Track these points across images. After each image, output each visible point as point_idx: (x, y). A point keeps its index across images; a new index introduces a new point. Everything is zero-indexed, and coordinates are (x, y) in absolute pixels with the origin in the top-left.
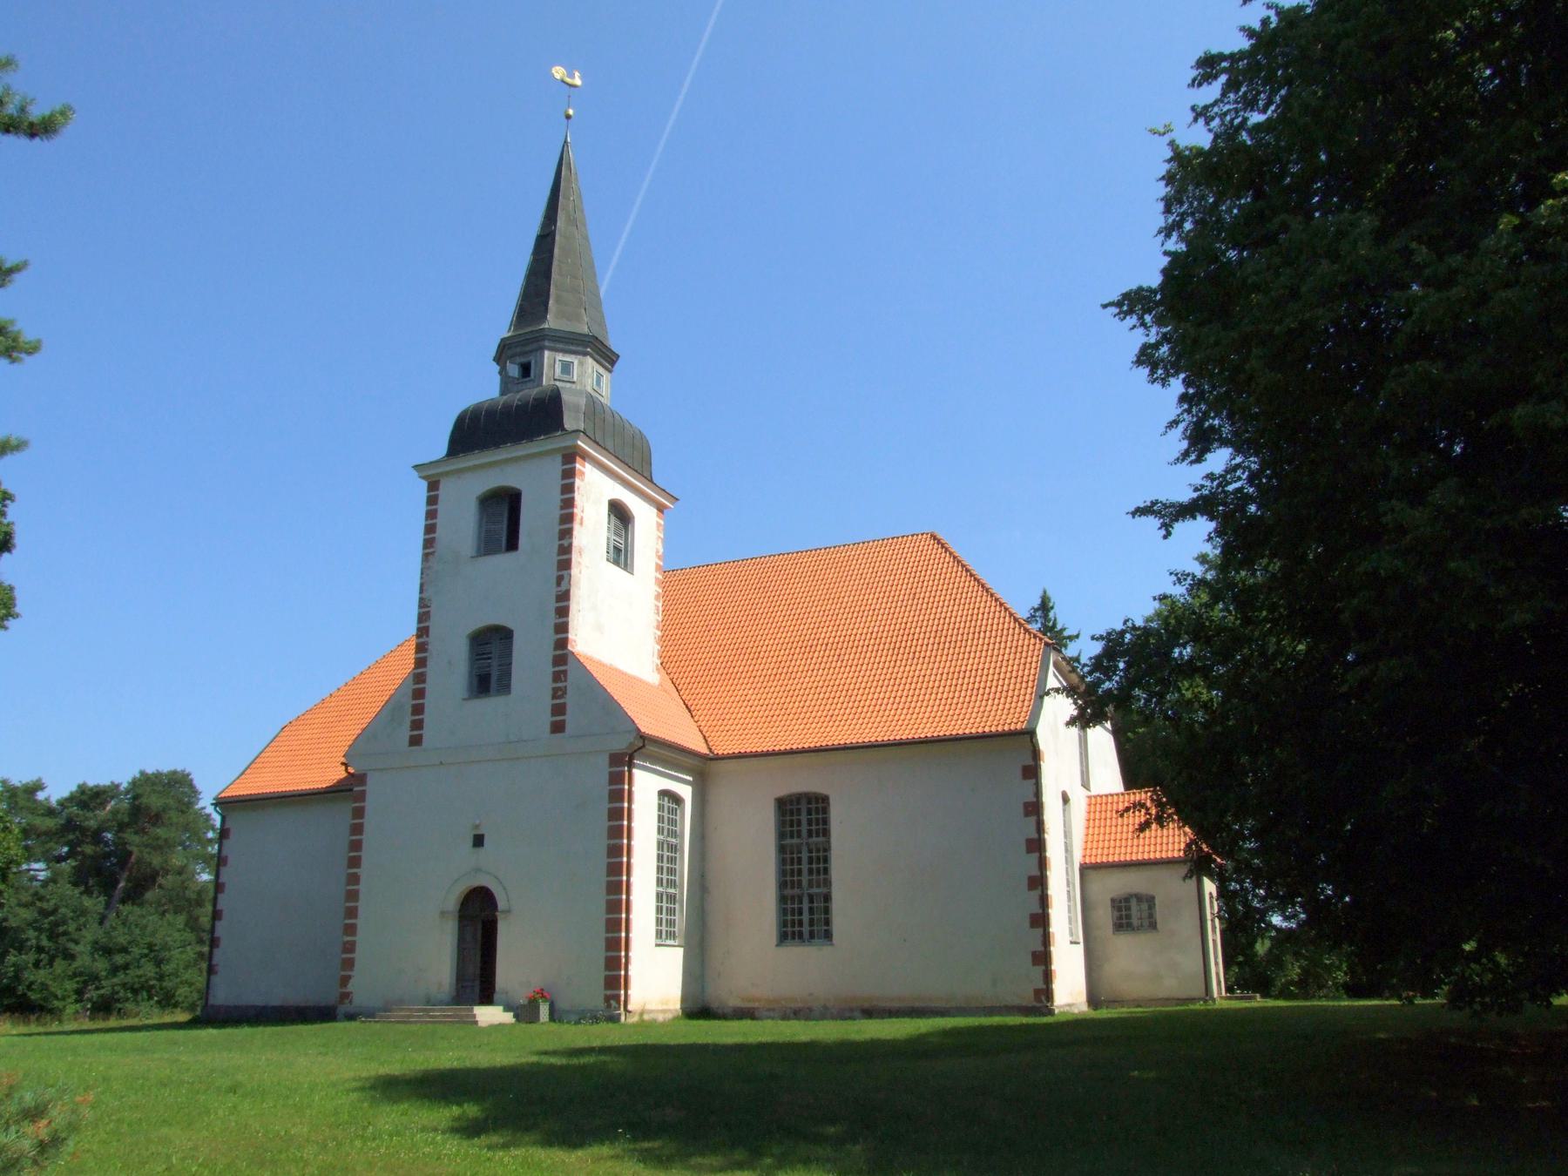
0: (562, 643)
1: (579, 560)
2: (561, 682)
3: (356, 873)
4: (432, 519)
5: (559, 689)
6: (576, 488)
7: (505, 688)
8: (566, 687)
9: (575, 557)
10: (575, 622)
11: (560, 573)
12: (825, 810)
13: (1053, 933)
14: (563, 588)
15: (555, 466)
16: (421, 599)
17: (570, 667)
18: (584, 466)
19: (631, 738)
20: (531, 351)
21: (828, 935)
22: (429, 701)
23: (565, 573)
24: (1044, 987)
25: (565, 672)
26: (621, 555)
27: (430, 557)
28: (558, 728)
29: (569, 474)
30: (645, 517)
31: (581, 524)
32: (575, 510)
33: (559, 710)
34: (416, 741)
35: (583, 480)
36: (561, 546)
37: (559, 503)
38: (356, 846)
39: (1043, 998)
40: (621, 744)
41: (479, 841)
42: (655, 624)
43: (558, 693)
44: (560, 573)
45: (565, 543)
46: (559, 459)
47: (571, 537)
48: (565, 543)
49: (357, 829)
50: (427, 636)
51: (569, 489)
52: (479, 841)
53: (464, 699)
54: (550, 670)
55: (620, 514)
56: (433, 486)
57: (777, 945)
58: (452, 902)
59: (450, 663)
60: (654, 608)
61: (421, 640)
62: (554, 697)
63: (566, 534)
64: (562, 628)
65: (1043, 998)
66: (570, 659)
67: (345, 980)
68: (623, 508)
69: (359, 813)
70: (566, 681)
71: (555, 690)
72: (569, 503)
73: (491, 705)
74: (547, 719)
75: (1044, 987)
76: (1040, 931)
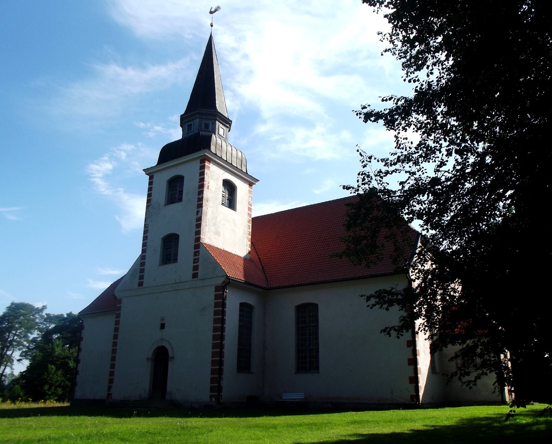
0: (198, 239)
1: (207, 204)
2: (197, 256)
3: (116, 342)
4: (150, 191)
5: (196, 259)
6: (205, 173)
7: (175, 260)
8: (199, 258)
9: (204, 202)
10: (204, 230)
11: (198, 209)
12: (179, 202)
13: (420, 368)
14: (199, 216)
15: (197, 164)
16: (145, 224)
17: (201, 250)
18: (210, 165)
19: (223, 279)
20: (192, 120)
21: (317, 368)
22: (146, 267)
23: (200, 209)
24: (415, 394)
25: (198, 252)
26: (231, 203)
27: (149, 207)
28: (195, 276)
29: (203, 167)
30: (241, 187)
31: (208, 188)
32: (205, 183)
33: (196, 268)
34: (141, 284)
35: (209, 170)
36: (199, 198)
37: (198, 180)
38: (116, 330)
39: (415, 400)
40: (220, 281)
41: (163, 326)
42: (248, 233)
43: (196, 261)
44: (198, 209)
45: (200, 196)
46: (199, 161)
47: (203, 194)
48: (200, 196)
49: (117, 323)
50: (147, 240)
51: (202, 174)
52: (163, 326)
53: (159, 265)
54: (193, 251)
55: (229, 186)
56: (151, 178)
57: (295, 373)
58: (150, 355)
59: (155, 250)
60: (247, 226)
61: (144, 242)
62: (194, 263)
63: (201, 192)
64: (198, 233)
65: (415, 400)
66: (201, 246)
67: (110, 388)
68: (233, 184)
69: (118, 316)
70: (199, 255)
71: (194, 259)
72: (202, 180)
73: (170, 267)
74: (191, 272)
75: (415, 394)
76: (413, 367)
